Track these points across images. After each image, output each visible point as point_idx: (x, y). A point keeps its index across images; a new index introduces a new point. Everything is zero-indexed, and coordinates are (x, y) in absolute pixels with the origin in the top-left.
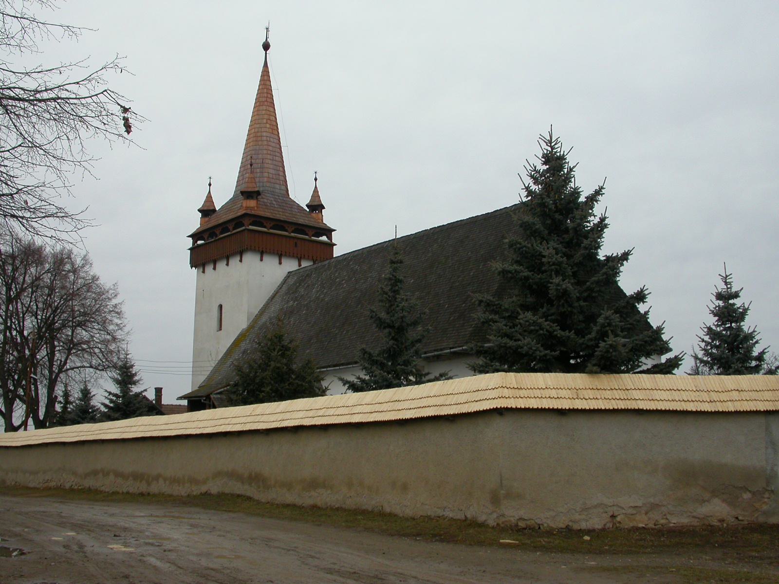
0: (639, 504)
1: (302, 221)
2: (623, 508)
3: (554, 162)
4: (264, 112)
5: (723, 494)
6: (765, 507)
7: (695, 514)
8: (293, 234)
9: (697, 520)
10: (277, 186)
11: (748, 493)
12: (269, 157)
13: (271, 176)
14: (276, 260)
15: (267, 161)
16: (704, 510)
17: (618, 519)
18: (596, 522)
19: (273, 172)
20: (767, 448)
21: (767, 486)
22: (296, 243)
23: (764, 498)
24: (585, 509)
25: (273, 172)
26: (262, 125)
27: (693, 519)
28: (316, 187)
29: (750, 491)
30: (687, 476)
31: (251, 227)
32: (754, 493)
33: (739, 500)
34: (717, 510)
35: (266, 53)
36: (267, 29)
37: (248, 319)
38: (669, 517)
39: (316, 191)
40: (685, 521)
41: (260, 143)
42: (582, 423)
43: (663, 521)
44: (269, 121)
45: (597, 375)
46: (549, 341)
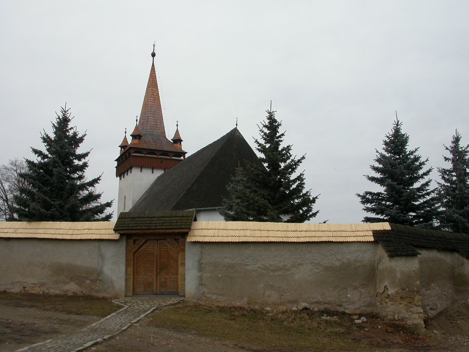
0: (36, 282)
1: (162, 148)
2: (29, 284)
3: (63, 123)
4: (150, 91)
5: (76, 280)
6: (97, 288)
7: (62, 289)
8: (160, 156)
9: (63, 292)
10: (156, 131)
11: (88, 280)
12: (151, 115)
13: (152, 125)
14: (150, 171)
15: (150, 118)
16: (66, 287)
17: (26, 289)
18: (16, 289)
19: (154, 123)
20: (98, 258)
21: (98, 277)
22: (162, 161)
23: (96, 283)
24: (13, 283)
25: (154, 123)
26: (149, 98)
27: (61, 292)
28: (177, 129)
29: (89, 279)
30: (59, 270)
31: (134, 154)
32: (91, 281)
33: (84, 283)
34: (72, 287)
35: (153, 59)
36: (154, 45)
37: (133, 203)
38: (50, 289)
39: (177, 132)
40: (57, 292)
41: (147, 108)
42: (16, 243)
43: (47, 291)
44: (152, 96)
45: (32, 222)
46: (47, 206)
